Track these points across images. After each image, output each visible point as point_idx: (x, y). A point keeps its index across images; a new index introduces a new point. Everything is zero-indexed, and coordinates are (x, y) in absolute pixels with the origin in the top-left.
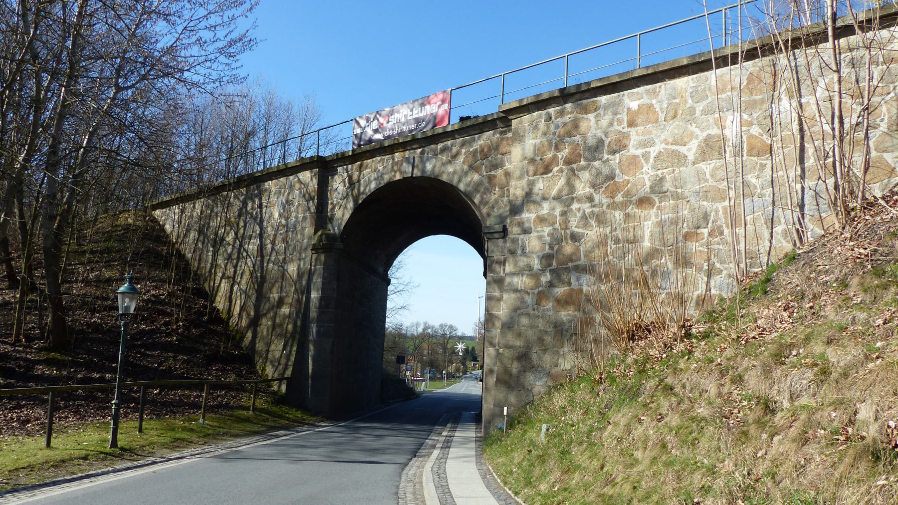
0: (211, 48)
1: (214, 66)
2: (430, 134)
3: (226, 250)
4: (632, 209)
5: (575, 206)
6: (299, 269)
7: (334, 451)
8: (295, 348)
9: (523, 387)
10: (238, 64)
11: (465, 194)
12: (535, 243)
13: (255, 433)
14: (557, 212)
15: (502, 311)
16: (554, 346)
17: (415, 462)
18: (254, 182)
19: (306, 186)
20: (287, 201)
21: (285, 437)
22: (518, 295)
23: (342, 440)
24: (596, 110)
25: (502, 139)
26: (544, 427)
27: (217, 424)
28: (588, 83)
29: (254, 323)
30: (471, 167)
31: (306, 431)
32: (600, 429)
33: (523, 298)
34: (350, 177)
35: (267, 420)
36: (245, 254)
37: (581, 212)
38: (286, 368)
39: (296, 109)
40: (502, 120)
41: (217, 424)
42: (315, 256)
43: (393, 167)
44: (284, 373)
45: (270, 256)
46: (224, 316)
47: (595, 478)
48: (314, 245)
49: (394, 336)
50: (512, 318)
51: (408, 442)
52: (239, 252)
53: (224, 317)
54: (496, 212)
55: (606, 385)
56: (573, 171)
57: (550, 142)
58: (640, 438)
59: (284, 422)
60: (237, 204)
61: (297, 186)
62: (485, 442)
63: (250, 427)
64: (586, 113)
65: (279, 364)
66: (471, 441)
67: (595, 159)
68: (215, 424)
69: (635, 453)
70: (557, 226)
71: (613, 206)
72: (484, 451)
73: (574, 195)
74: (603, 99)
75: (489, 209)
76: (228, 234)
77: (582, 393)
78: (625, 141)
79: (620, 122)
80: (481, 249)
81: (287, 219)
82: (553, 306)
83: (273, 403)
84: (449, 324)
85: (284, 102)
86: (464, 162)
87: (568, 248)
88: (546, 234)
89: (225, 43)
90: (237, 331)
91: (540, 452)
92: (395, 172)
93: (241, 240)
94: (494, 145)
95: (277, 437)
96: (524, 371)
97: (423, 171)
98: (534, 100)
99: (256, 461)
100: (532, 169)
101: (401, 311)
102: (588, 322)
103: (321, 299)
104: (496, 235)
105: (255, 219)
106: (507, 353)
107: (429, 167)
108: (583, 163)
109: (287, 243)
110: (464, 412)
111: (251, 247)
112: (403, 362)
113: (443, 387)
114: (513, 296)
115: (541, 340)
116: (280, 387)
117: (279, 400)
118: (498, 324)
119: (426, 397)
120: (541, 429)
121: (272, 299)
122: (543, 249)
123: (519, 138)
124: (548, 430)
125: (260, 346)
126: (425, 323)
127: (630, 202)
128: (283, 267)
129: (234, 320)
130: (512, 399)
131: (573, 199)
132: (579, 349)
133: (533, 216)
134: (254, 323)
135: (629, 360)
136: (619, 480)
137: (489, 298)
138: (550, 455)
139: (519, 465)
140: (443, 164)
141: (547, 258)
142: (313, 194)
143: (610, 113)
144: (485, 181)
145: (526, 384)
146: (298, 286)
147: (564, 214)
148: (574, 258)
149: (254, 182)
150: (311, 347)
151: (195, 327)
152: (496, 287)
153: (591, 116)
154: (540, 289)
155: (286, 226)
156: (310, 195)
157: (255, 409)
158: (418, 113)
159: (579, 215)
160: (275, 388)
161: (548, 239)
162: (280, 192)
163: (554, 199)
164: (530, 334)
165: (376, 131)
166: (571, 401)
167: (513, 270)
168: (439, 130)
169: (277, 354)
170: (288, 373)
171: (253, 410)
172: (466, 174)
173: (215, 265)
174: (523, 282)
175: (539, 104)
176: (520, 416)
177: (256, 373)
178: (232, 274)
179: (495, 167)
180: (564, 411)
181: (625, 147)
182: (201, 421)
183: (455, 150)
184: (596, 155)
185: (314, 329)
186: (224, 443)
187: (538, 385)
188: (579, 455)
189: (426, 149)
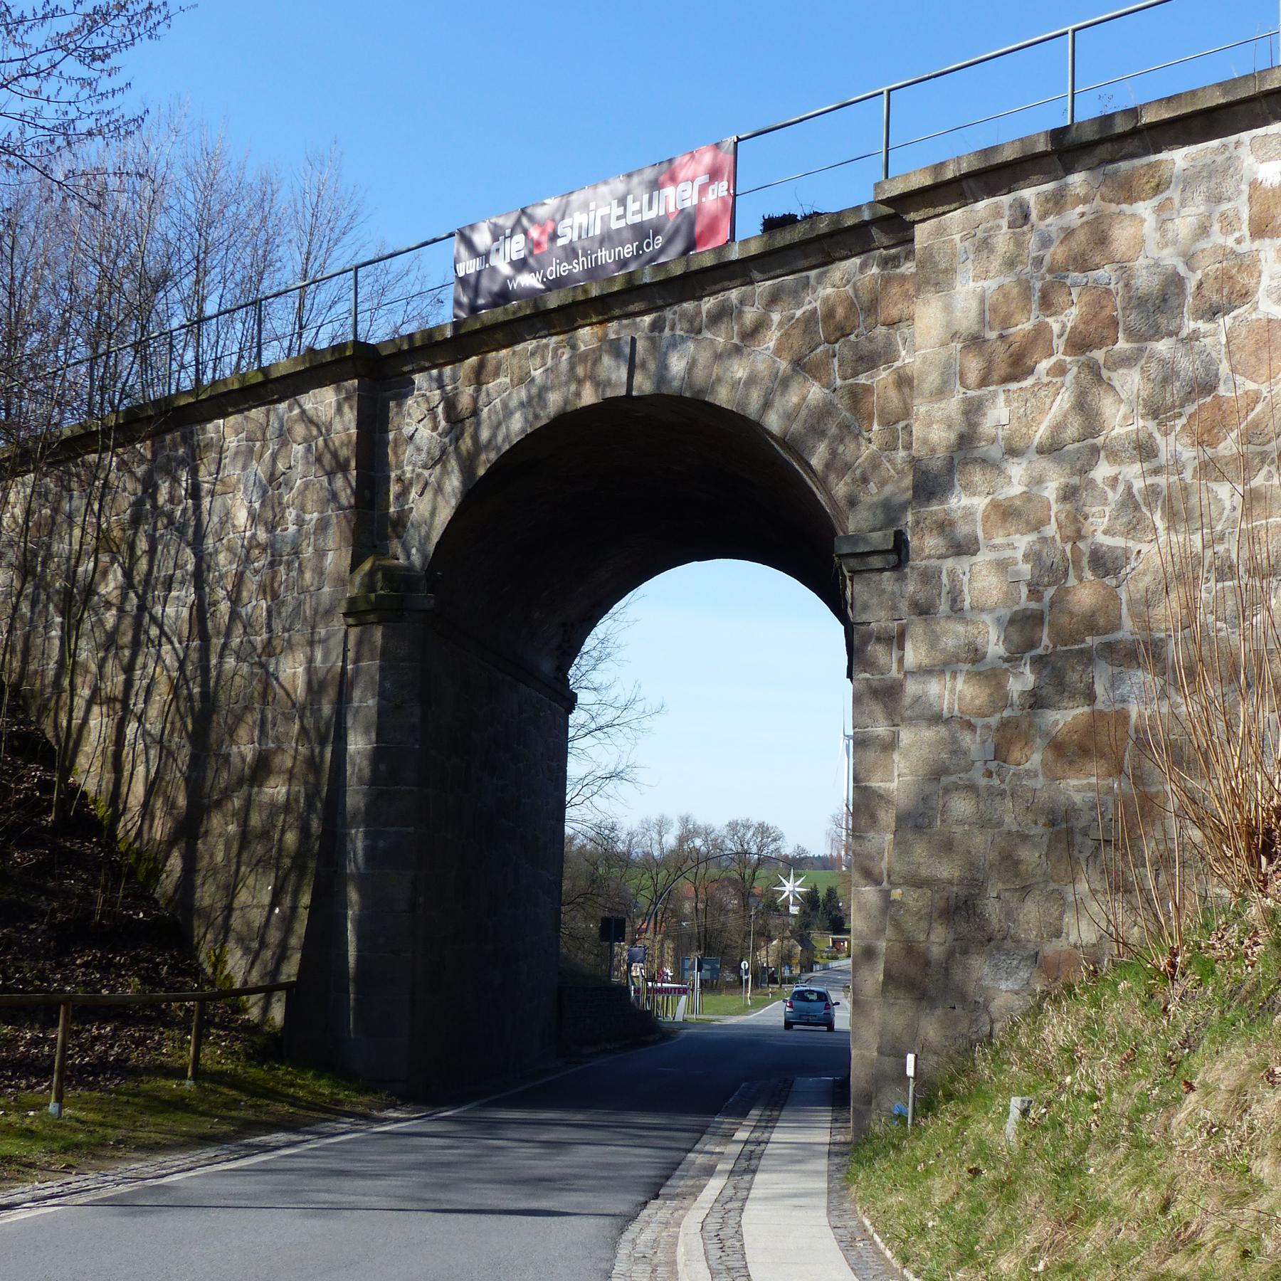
0: (38, 37)
1: (49, 88)
2: (678, 270)
3: (101, 622)
4: (1269, 476)
5: (1102, 471)
6: (310, 670)
7: (426, 1185)
8: (306, 899)
9: (963, 998)
10: (117, 81)
11: (782, 441)
12: (987, 581)
13: (204, 1140)
14: (1051, 491)
15: (898, 779)
16: (1048, 879)
17: (657, 1211)
18: (171, 424)
19: (324, 429)
20: (272, 477)
21: (286, 1150)
22: (943, 731)
23: (451, 1155)
24: (1157, 189)
25: (887, 281)
26: (1016, 1103)
27: (98, 1117)
28: (1134, 113)
29: (189, 830)
30: (801, 366)
31: (346, 1135)
32: (1165, 1104)
33: (954, 740)
34: (450, 404)
35: (232, 1104)
36: (154, 632)
37: (1121, 487)
38: (282, 955)
39: (283, 199)
40: (887, 225)
41: (98, 1117)
42: (354, 633)
43: (572, 368)
44: (276, 971)
45: (228, 635)
46: (102, 811)
47: (1144, 1236)
48: (352, 601)
49: (592, 860)
50: (925, 799)
51: (638, 1158)
52: (138, 626)
53: (100, 813)
54: (873, 493)
55: (1188, 983)
56: (1094, 370)
57: (1026, 289)
58: (1269, 1123)
59: (284, 1109)
60: (127, 491)
61: (300, 430)
62: (852, 1156)
63: (186, 1123)
64: (1131, 199)
65: (263, 944)
66: (816, 1155)
67: (1157, 334)
68: (91, 1116)
69: (1256, 1165)
70: (1051, 530)
71: (1208, 469)
72: (850, 1179)
73: (1100, 440)
74: (1179, 158)
75: (854, 483)
76: (105, 574)
77: (1123, 1008)
78: (1243, 279)
79: (1229, 224)
80: (833, 596)
81: (271, 528)
82: (1044, 763)
83: (249, 1057)
84: (755, 820)
85: (251, 177)
86: (778, 351)
87: (1085, 594)
88: (1019, 555)
89: (77, 21)
90: (139, 853)
91: (1003, 1173)
92: (580, 382)
93: (143, 589)
94: (866, 297)
95: (265, 1149)
96: (965, 952)
97: (662, 376)
98: (976, 165)
99: (213, 1213)
100: (974, 366)
101: (610, 787)
102: (1146, 807)
103: (377, 755)
104: (876, 562)
105: (181, 530)
106: (913, 900)
107: (677, 365)
108: (1123, 345)
109: (275, 596)
110: (794, 1076)
111: (170, 611)
112: (620, 936)
113: (744, 1010)
114: (929, 734)
115: (1009, 862)
116: (266, 1009)
117: (268, 1048)
118: (887, 818)
119: (690, 1038)
120: (1007, 1111)
121: (236, 760)
122: (1010, 597)
123: (936, 277)
124: (1025, 1113)
125: (206, 895)
126: (685, 821)
127: (1263, 457)
128: (263, 666)
129: (128, 825)
130: (931, 1030)
131: (1095, 451)
132: (1121, 887)
133: (979, 503)
134: (189, 830)
135: (1253, 913)
136: (1207, 1236)
137: (861, 743)
138: (1027, 1179)
139: (945, 1212)
140: (718, 357)
141: (1023, 626)
142: (344, 452)
143: (1199, 199)
144: (842, 404)
145: (971, 988)
146: (309, 722)
147: (1069, 494)
148: (1102, 622)
149: (171, 424)
150: (353, 895)
151: (22, 847)
152: (877, 709)
153: (1144, 209)
154: (1006, 714)
155: (271, 547)
156: (335, 455)
157: (199, 1074)
158: (641, 211)
159: (1114, 497)
160: (254, 1014)
161: (1026, 569)
162: (251, 450)
163: (1041, 451)
164: (980, 842)
165: (521, 265)
166: (1090, 1028)
167: (926, 661)
168: (704, 257)
169: (257, 917)
170: (290, 970)
171: (195, 1077)
172: (785, 383)
173: (68, 664)
174: (952, 692)
175: (993, 176)
176: (953, 1079)
177: (197, 972)
178: (119, 691)
179: (868, 360)
180: (1071, 1058)
181: (1245, 295)
182: (52, 1107)
183: (750, 315)
184: (1163, 321)
185: (358, 840)
186: (122, 1166)
187: (1004, 989)
188: (1106, 1176)
189: (668, 314)
